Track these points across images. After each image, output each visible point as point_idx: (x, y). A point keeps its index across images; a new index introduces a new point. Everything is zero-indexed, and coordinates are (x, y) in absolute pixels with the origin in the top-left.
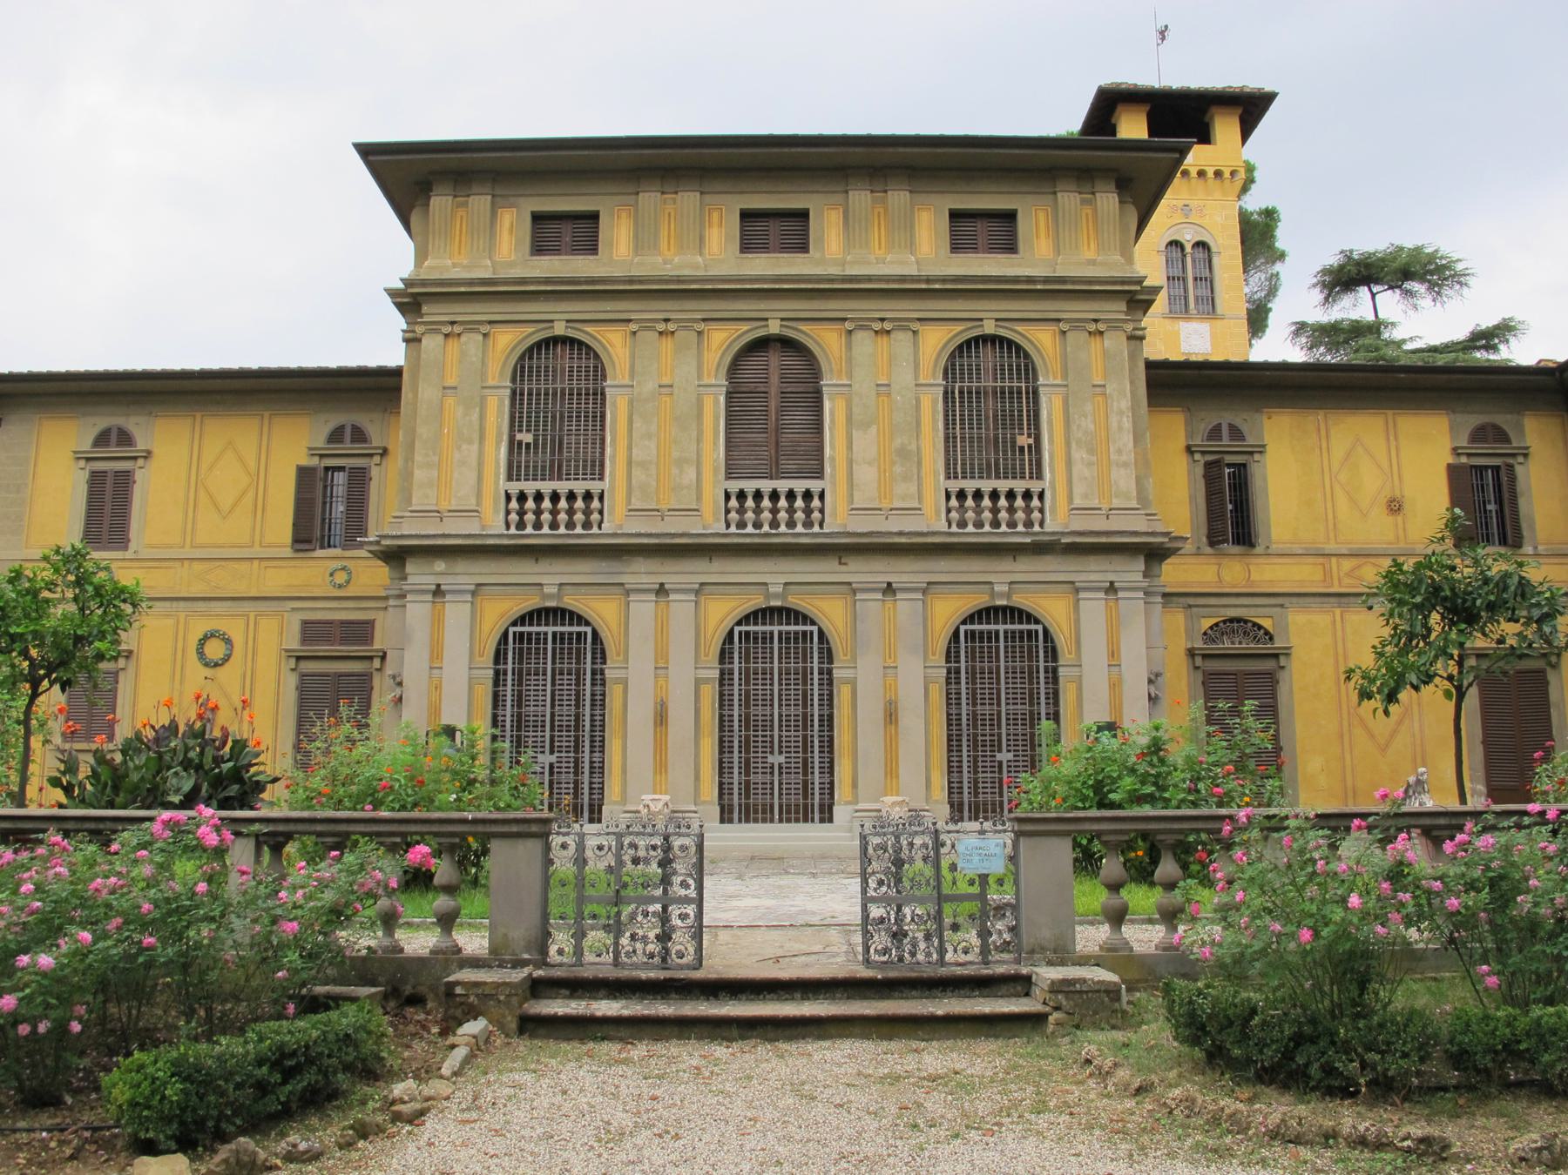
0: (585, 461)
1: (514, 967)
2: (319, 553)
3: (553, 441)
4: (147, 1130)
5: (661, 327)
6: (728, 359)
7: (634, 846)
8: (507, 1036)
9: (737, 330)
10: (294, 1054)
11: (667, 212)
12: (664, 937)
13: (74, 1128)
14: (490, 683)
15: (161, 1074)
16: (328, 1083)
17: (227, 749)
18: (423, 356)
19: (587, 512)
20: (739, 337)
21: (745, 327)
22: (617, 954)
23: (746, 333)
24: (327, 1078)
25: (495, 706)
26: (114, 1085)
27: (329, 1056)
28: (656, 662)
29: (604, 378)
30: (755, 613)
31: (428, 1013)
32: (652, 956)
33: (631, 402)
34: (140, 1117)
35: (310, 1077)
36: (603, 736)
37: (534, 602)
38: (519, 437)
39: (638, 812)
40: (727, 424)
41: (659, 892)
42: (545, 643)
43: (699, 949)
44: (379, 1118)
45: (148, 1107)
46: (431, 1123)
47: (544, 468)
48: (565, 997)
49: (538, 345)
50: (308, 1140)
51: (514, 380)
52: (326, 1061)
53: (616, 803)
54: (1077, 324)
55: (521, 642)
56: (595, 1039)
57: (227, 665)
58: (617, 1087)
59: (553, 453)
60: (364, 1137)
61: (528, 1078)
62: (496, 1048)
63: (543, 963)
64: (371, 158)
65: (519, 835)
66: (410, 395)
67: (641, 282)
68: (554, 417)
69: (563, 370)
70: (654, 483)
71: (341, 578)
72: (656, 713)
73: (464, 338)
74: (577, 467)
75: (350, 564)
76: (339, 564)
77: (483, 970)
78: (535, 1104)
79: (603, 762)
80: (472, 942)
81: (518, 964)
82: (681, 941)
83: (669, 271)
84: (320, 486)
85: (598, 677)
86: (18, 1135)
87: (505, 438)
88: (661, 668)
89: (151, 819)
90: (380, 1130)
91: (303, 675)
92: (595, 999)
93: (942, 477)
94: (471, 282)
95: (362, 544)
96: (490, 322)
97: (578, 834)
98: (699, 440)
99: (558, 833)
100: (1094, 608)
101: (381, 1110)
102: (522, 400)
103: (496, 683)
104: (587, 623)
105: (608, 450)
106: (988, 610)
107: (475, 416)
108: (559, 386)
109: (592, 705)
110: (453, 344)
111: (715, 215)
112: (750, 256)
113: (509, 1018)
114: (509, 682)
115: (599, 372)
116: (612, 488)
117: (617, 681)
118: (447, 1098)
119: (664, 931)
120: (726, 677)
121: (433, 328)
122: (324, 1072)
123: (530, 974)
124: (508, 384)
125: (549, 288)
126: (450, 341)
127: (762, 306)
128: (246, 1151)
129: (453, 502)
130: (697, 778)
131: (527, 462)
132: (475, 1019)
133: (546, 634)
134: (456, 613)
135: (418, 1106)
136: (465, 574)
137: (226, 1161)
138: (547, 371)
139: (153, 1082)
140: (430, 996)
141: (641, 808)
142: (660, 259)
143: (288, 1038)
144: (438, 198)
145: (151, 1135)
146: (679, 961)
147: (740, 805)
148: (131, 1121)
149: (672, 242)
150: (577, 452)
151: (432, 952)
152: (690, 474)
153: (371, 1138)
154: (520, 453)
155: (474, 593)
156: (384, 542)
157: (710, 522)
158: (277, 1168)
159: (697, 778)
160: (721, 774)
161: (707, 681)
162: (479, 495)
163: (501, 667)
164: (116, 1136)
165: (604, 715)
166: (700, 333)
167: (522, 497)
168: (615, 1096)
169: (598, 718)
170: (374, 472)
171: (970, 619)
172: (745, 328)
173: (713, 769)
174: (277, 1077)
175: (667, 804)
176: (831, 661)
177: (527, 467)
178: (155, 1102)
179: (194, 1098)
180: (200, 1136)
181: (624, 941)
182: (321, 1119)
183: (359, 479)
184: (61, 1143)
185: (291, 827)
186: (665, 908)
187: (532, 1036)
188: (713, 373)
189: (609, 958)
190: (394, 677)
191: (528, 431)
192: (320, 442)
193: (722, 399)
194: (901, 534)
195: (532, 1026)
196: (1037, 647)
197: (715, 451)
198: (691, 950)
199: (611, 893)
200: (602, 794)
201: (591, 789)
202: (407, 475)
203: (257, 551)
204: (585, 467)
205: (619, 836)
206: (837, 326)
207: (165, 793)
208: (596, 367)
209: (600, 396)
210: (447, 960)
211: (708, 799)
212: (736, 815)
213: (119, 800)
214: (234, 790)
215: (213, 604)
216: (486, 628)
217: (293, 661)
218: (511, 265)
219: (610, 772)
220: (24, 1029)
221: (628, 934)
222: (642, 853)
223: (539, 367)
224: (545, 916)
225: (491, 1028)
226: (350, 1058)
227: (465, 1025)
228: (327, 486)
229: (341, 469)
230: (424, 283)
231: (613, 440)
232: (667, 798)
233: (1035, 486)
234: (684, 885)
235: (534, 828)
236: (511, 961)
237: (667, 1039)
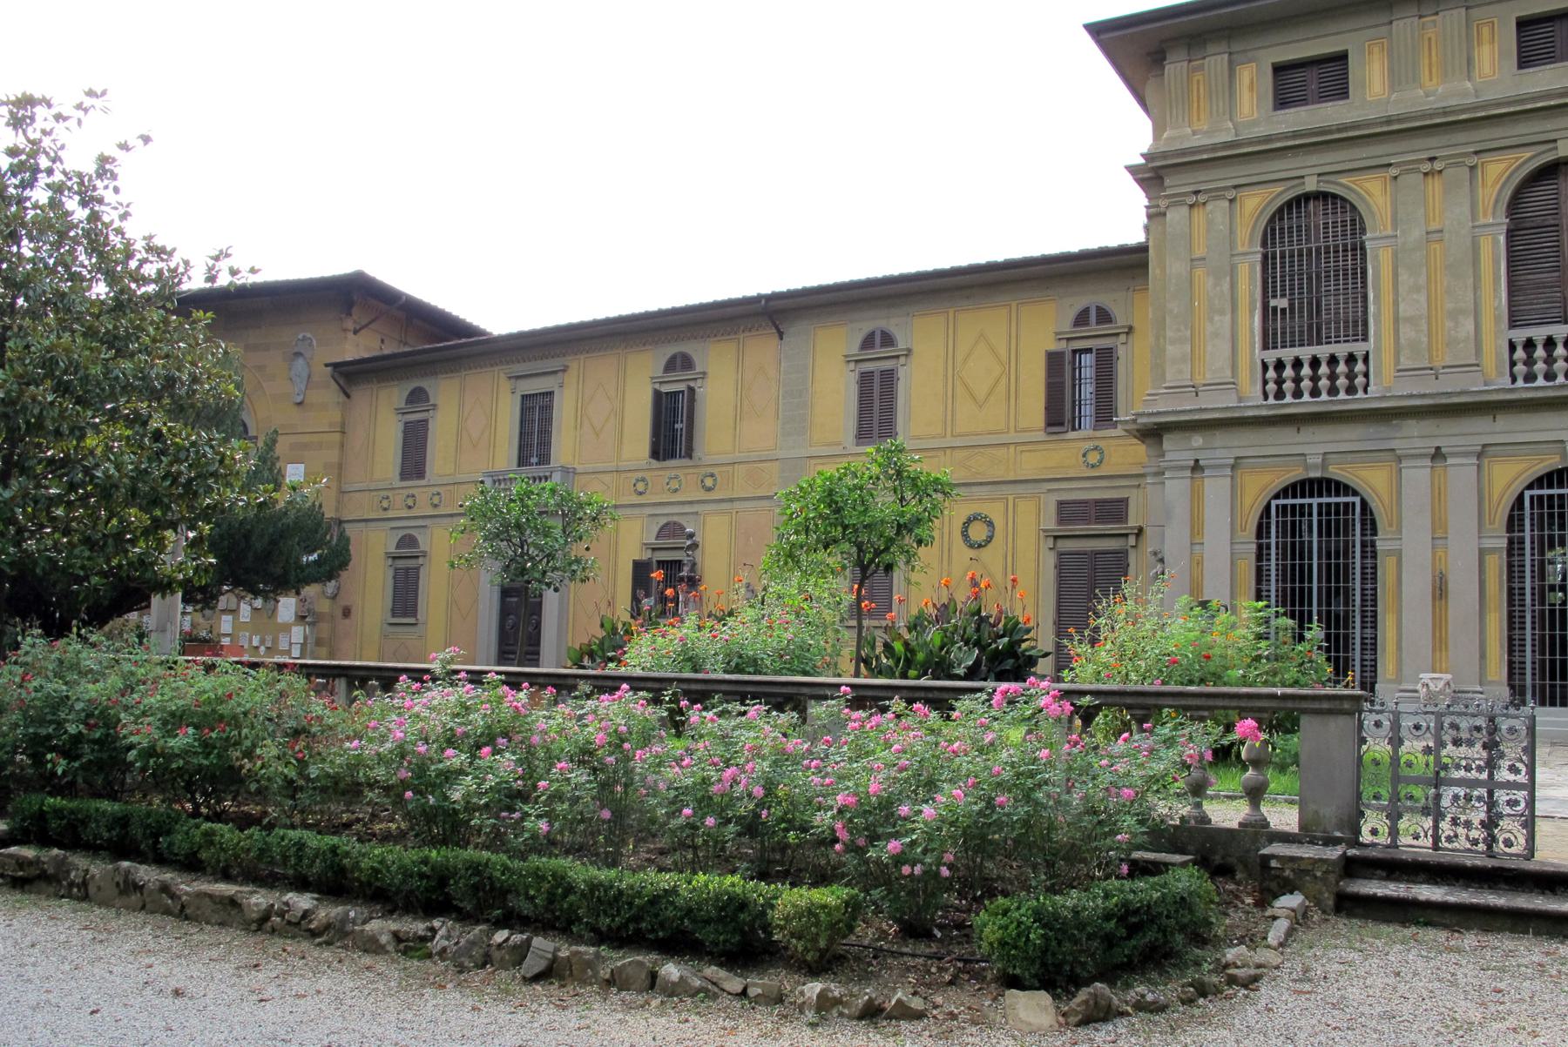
0: (1346, 322)
1: (1326, 844)
2: (1072, 435)
3: (1310, 303)
4: (1014, 967)
5: (1426, 167)
6: (1508, 193)
7: (1455, 726)
8: (1324, 912)
9: (1517, 159)
10: (1137, 912)
11: (1426, 37)
12: (1490, 824)
13: (948, 958)
14: (1253, 557)
15: (1024, 919)
16: (1166, 942)
17: (1001, 626)
18: (1169, 230)
19: (1351, 376)
20: (1273, 199)
21: (1527, 154)
22: (1436, 838)
23: (1280, 194)
24: (1165, 936)
25: (1259, 580)
26: (985, 925)
27: (1168, 917)
28: (1434, 531)
29: (1363, 231)
30: (1550, 475)
31: (1238, 883)
32: (1475, 842)
33: (1395, 255)
34: (1008, 955)
35: (1151, 935)
36: (1376, 612)
37: (1295, 474)
38: (1273, 303)
39: (1416, 691)
40: (1508, 267)
41: (1484, 776)
42: (1310, 515)
43: (1531, 839)
44: (1215, 979)
45: (1016, 947)
46: (1265, 991)
47: (1301, 332)
48: (1381, 879)
49: (1289, 204)
50: (1153, 992)
51: (1264, 244)
52: (1164, 921)
53: (1390, 681)
54: (1410, 168)
55: (1541, 506)
56: (1417, 923)
57: (990, 546)
58: (1453, 975)
59: (1310, 316)
60: (1204, 995)
61: (1354, 955)
62: (1314, 923)
63: (1356, 843)
64: (1102, 37)
65: (1330, 712)
66: (1158, 271)
67: (1400, 121)
68: (1310, 279)
69: (1317, 227)
70: (1425, 339)
71: (1093, 458)
72: (1434, 588)
73: (1209, 207)
74: (1337, 329)
75: (1101, 444)
76: (1089, 445)
77: (1294, 846)
78: (1368, 982)
79: (1375, 638)
80: (1284, 817)
81: (1330, 841)
82: (1511, 829)
83: (1433, 103)
84: (1068, 368)
85: (1369, 549)
86: (906, 959)
87: (1259, 305)
88: (1439, 535)
89: (980, 690)
90: (1217, 991)
91: (1061, 554)
92: (1415, 882)
93: (1258, 345)
94: (1214, 148)
95: (1115, 425)
96: (1236, 187)
97: (1392, 712)
98: (1476, 288)
99: (1370, 711)
100: (1418, 476)
101: (1215, 971)
102: (1274, 264)
103: (1259, 558)
104: (1355, 493)
105: (1372, 308)
106: (1303, 483)
107: (1226, 286)
108: (1313, 245)
109: (1363, 579)
110: (1199, 216)
111: (1486, 31)
112: (1531, 70)
113: (1326, 895)
114: (1273, 557)
115: (1357, 225)
116: (1378, 348)
117: (1390, 553)
118: (1277, 968)
119: (1489, 818)
120: (1516, 546)
121: (1176, 201)
122: (1163, 930)
123: (1345, 853)
124: (1259, 249)
125: (1297, 142)
126: (1196, 210)
127: (1549, 127)
128: (1103, 995)
129: (1207, 376)
130: (1483, 656)
131: (1292, 327)
132: (1292, 893)
133: (1310, 505)
134: (1216, 488)
135: (1252, 971)
136: (1224, 447)
137: (1086, 1002)
138: (1299, 231)
139: (1018, 926)
140: (1240, 867)
141: (1419, 687)
142: (1421, 92)
143: (1131, 896)
144: (1172, 66)
145: (1018, 971)
146: (1507, 850)
147: (1534, 686)
148: (1001, 958)
149: (1434, 70)
150: (1337, 313)
151: (1240, 824)
152: (1469, 325)
153: (1210, 998)
154: (1275, 320)
155: (1233, 467)
156: (1141, 420)
157: (1494, 378)
158: (1128, 1014)
159: (1483, 656)
160: (1511, 652)
161: (1493, 550)
162: (1234, 367)
163: (1264, 541)
164: (984, 969)
165: (1375, 589)
166: (1473, 168)
167: (1280, 366)
168: (1454, 984)
169: (1369, 592)
170: (1121, 352)
171: (1539, 482)
172: (1528, 155)
173: (1501, 646)
174: (1123, 932)
175: (1448, 683)
176: (1374, 532)
177: (1283, 333)
178: (1021, 944)
179: (1054, 943)
180: (1058, 978)
181: (1445, 825)
182: (1161, 975)
183: (1106, 360)
184: (940, 969)
185: (710, 687)
186: (1491, 794)
187: (1350, 915)
188: (1490, 210)
189: (1429, 842)
190: (1155, 554)
191: (1283, 296)
192: (1066, 325)
193: (1502, 239)
194: (1411, 396)
195: (1350, 906)
196: (1354, 520)
197: (1496, 297)
198: (1522, 840)
199: (1430, 774)
200: (1375, 671)
201: (1362, 666)
202: (1159, 352)
203: (1012, 437)
204: (1346, 327)
205: (1439, 716)
206: (1382, 173)
207: (951, 666)
208: (1353, 221)
209: (1359, 250)
210: (1256, 834)
211: (1496, 678)
212: (1529, 696)
213: (912, 673)
214: (1009, 664)
215: (974, 489)
216: (1248, 501)
217: (1051, 540)
218: (1255, 123)
219: (1384, 650)
220: (906, 870)
221: (1448, 819)
222: (1464, 735)
223: (1290, 228)
224: (1359, 795)
225: (1307, 903)
226: (1185, 920)
227: (1282, 898)
228: (1076, 368)
229: (1089, 351)
230: (1164, 155)
231: (1377, 297)
232: (1449, 676)
233: (1358, 348)
234: (1513, 769)
235: (1346, 706)
236: (1322, 839)
237: (1499, 930)
